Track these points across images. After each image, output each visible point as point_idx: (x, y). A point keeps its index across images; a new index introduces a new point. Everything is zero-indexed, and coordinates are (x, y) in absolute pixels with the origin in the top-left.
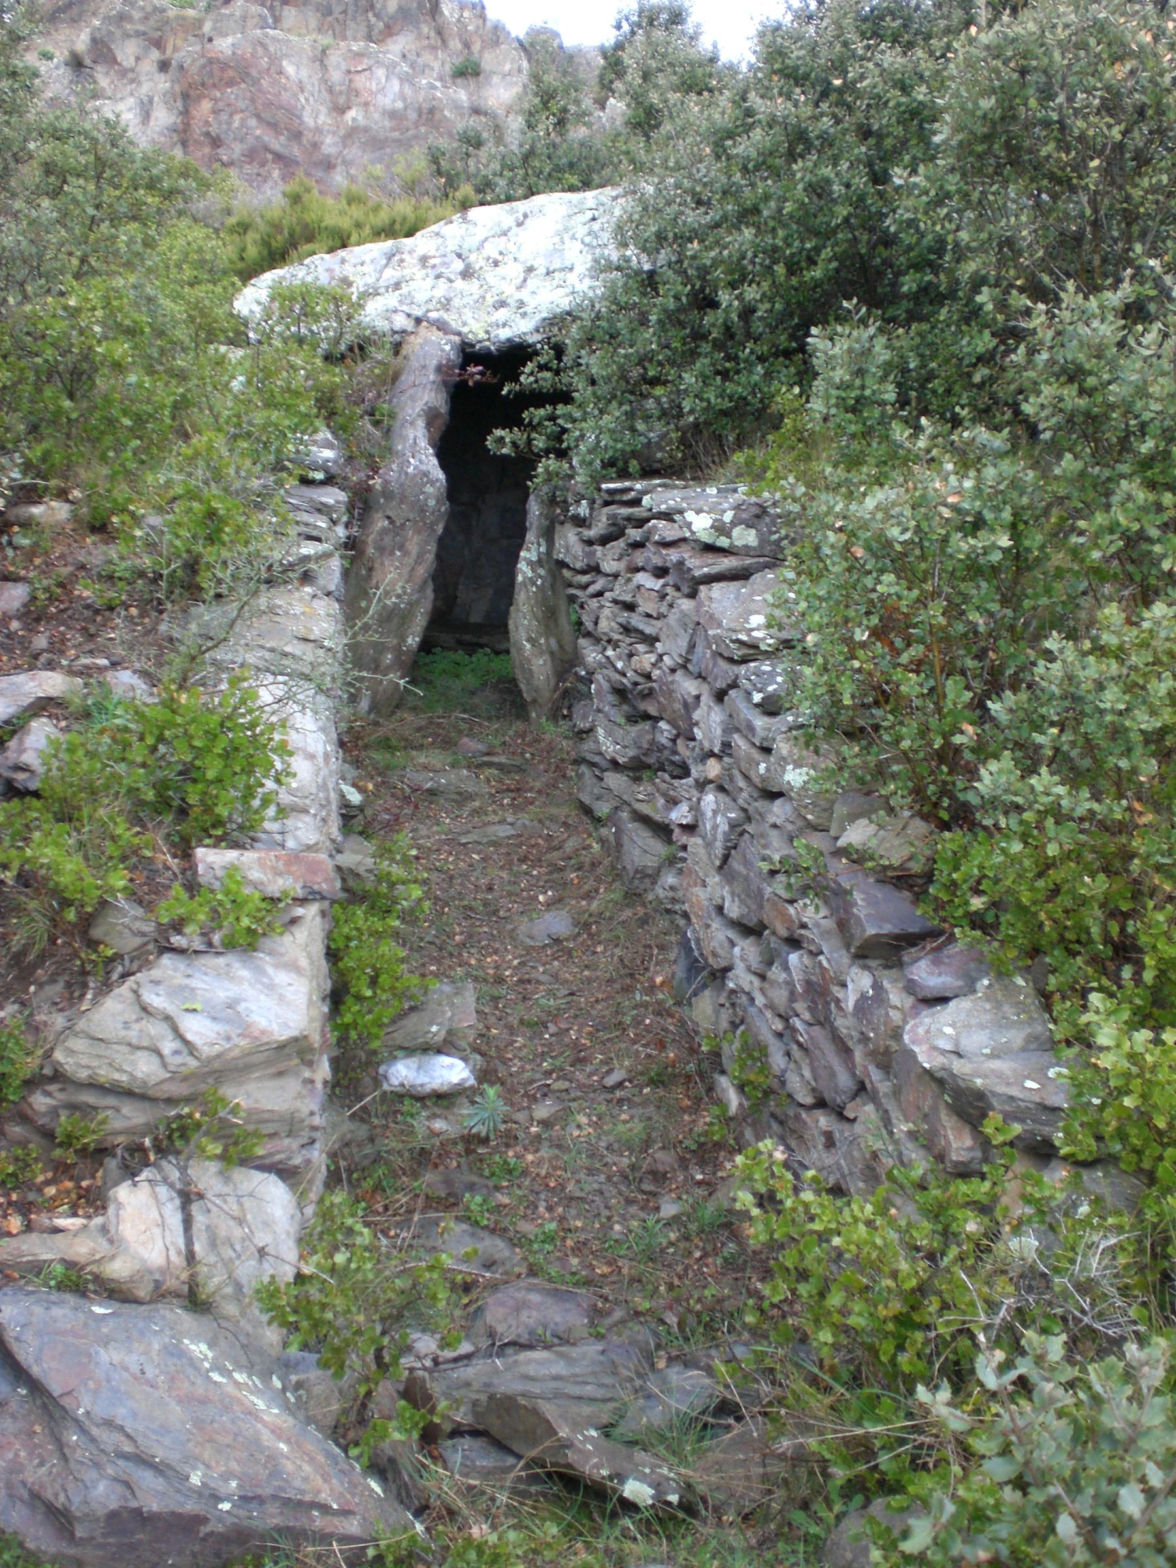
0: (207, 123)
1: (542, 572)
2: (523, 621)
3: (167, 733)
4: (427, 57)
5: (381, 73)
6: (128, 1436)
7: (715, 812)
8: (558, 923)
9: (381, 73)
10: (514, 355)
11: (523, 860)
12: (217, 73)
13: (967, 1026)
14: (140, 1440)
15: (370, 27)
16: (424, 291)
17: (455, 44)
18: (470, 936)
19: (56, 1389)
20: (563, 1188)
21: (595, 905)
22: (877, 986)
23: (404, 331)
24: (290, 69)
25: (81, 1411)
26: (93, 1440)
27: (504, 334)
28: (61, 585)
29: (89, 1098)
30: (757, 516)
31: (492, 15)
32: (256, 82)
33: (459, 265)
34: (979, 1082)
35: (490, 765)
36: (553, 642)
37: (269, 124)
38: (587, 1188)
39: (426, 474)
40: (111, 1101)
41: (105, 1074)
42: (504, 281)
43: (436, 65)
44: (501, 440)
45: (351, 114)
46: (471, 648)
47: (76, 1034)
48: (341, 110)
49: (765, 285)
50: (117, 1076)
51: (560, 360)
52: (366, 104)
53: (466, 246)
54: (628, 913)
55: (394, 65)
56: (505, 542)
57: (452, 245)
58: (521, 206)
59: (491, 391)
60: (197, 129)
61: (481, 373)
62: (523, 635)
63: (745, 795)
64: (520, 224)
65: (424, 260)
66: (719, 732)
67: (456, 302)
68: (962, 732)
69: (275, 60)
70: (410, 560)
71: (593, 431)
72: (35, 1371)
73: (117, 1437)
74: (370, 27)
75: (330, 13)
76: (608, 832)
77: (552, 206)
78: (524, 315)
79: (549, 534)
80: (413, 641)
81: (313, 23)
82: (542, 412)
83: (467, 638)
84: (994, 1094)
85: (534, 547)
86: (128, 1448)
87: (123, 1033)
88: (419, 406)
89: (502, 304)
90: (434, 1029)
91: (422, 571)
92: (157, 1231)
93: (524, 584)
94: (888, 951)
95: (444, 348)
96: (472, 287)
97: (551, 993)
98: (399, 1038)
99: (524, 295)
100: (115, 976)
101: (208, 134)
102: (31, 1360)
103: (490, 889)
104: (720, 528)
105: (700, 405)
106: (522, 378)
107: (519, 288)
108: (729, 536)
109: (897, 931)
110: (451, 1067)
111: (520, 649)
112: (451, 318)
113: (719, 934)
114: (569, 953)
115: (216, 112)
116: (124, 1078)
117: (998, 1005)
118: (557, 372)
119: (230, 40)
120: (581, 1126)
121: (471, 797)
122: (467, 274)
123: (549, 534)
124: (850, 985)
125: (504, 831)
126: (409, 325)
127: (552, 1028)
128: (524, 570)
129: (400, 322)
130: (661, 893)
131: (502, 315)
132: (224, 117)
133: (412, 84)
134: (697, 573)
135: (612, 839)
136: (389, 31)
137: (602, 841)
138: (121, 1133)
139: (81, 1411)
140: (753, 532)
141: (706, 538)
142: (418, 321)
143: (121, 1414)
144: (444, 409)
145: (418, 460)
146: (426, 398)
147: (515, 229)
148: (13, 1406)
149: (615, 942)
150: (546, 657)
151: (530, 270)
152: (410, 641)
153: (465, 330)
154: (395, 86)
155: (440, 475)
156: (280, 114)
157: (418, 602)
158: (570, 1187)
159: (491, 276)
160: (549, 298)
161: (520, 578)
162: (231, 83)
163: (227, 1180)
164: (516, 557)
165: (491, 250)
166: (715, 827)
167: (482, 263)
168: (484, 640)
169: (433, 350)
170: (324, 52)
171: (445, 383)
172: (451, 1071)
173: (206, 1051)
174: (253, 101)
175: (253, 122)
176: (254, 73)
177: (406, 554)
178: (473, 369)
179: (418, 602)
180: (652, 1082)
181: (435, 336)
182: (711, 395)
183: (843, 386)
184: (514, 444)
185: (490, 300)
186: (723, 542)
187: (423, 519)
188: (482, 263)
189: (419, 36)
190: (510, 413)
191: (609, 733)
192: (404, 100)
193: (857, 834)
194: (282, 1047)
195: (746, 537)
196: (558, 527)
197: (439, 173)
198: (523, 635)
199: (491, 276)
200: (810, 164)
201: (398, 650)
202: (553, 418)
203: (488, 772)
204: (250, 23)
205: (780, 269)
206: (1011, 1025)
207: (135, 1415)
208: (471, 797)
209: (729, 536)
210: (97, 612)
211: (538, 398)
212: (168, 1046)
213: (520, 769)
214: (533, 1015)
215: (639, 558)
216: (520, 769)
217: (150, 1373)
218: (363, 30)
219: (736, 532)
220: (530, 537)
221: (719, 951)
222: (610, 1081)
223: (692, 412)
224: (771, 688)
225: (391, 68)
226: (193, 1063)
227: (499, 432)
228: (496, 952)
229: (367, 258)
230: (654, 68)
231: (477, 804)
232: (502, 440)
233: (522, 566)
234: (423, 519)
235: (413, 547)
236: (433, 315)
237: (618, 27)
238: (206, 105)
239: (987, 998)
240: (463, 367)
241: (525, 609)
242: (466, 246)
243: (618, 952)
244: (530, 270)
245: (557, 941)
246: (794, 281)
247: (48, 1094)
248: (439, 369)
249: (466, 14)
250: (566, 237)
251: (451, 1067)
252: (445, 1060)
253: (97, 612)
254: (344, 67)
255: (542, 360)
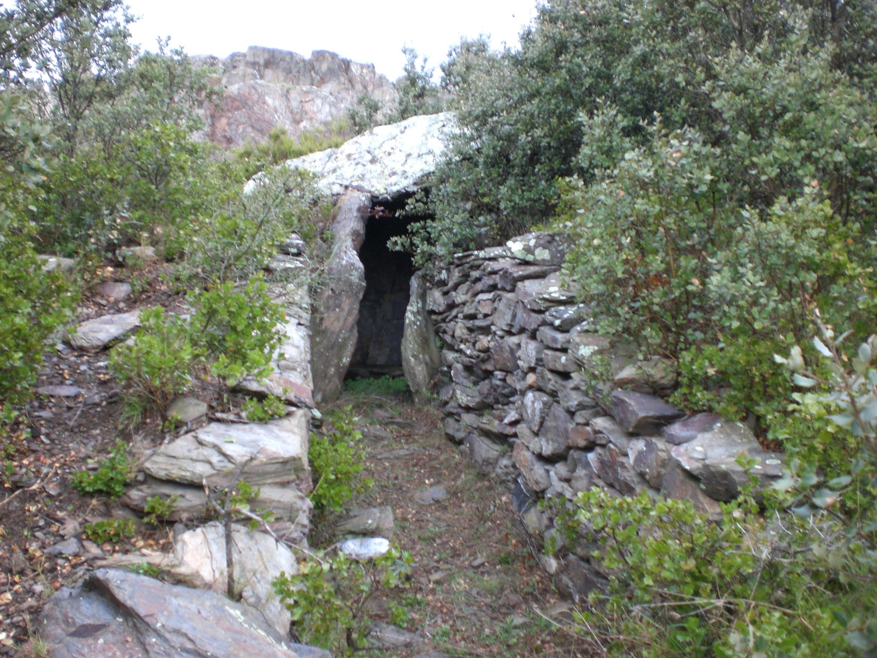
0: (225, 130)
1: (420, 318)
2: (410, 346)
3: (214, 97)
4: (344, 94)
5: (319, 102)
6: (190, 640)
7: (533, 403)
8: (439, 493)
9: (319, 102)
10: (401, 198)
11: (414, 466)
12: (230, 103)
13: (711, 446)
14: (197, 642)
15: (312, 79)
16: (349, 172)
17: (359, 87)
18: (386, 500)
19: (142, 612)
20: (452, 612)
21: (459, 482)
22: (648, 445)
23: (338, 194)
24: (269, 101)
25: (159, 625)
26: (166, 640)
27: (395, 189)
28: (149, 284)
29: (166, 490)
30: (549, 242)
31: (379, 71)
32: (251, 108)
33: (369, 157)
34: (723, 467)
35: (393, 423)
36: (427, 358)
37: (258, 130)
38: (466, 613)
39: (353, 265)
40: (179, 492)
41: (176, 473)
42: (395, 162)
43: (349, 98)
44: (396, 243)
45: (303, 124)
46: (378, 376)
47: (159, 455)
48: (297, 122)
49: (546, 129)
50: (183, 473)
51: (427, 197)
52: (311, 119)
53: (372, 147)
54: (479, 484)
55: (326, 97)
56: (395, 322)
57: (365, 147)
58: (404, 123)
59: (387, 222)
60: (219, 134)
61: (383, 211)
62: (409, 353)
63: (553, 382)
64: (402, 132)
65: (349, 156)
66: (534, 353)
67: (368, 176)
68: (692, 284)
69: (261, 96)
70: (345, 314)
71: (451, 221)
72: (129, 603)
73: (183, 640)
74: (312, 79)
75: (291, 72)
76: (465, 447)
77: (419, 123)
78: (406, 178)
79: (423, 297)
80: (346, 360)
81: (282, 78)
82: (418, 224)
83: (376, 370)
84: (734, 472)
85: (415, 304)
86: (189, 646)
87: (187, 454)
88: (348, 230)
89: (394, 173)
90: (370, 521)
91: (351, 320)
92: (208, 561)
93: (410, 324)
94: (654, 427)
95: (362, 199)
96: (377, 167)
97: (435, 526)
98: (350, 525)
99: (406, 168)
100: (182, 432)
101: (225, 137)
102: (127, 597)
103: (396, 478)
104: (528, 250)
105: (510, 204)
106: (407, 208)
107: (403, 165)
108: (533, 254)
109: (658, 414)
110: (381, 544)
111: (408, 361)
112: (365, 185)
113: (539, 469)
114: (445, 508)
115: (229, 124)
116: (188, 474)
117: (728, 435)
118: (426, 203)
119: (237, 86)
120: (461, 584)
121: (382, 439)
122: (373, 161)
123: (423, 297)
124: (630, 452)
125: (402, 452)
126: (341, 190)
127: (438, 541)
128: (409, 316)
129: (337, 189)
130: (499, 470)
131: (394, 179)
132: (234, 127)
133: (335, 107)
134: (515, 275)
135: (467, 450)
136: (323, 81)
137: (462, 453)
138: (184, 511)
139: (159, 625)
140: (547, 251)
141: (519, 255)
142: (346, 187)
143: (185, 628)
144: (362, 232)
145: (348, 257)
146: (352, 225)
147: (400, 135)
148: (113, 627)
149: (470, 499)
150: (423, 365)
151: (409, 155)
152: (344, 360)
153: (373, 189)
154: (327, 108)
155: (361, 265)
156: (264, 125)
157: (349, 338)
158: (456, 612)
159: (387, 160)
160: (418, 168)
161: (407, 321)
162: (237, 109)
163: (252, 537)
164: (405, 311)
165: (387, 147)
166: (534, 410)
167: (382, 155)
168: (385, 371)
169: (356, 200)
170: (288, 92)
171: (362, 218)
172: (379, 546)
173: (239, 459)
174: (249, 118)
175: (249, 129)
176: (250, 103)
177: (342, 310)
178: (378, 208)
179: (349, 338)
180: (500, 563)
181: (356, 194)
182: (517, 199)
183: (602, 139)
184: (402, 244)
185: (387, 172)
186: (530, 258)
187: (351, 290)
188: (382, 155)
189: (339, 83)
190: (400, 227)
191: (463, 392)
192: (332, 115)
193: (628, 372)
194: (285, 462)
195: (543, 254)
196: (428, 292)
197: (355, 124)
198: (409, 353)
199: (387, 160)
200: (569, 57)
201: (338, 367)
202: (424, 228)
203: (391, 427)
204: (247, 78)
205: (554, 121)
206: (736, 444)
207: (194, 629)
208: (382, 439)
209: (533, 254)
210: (170, 296)
211: (416, 218)
212: (215, 458)
213: (410, 425)
214: (427, 534)
215: (479, 286)
216: (410, 425)
217: (204, 613)
218: (309, 81)
219: (537, 252)
220: (413, 299)
221: (540, 480)
222: (476, 563)
223: (505, 209)
224: (565, 316)
225: (324, 99)
226: (231, 466)
227: (394, 239)
228: (402, 507)
229: (317, 159)
230: (470, 60)
231: (386, 442)
232: (396, 243)
233: (408, 315)
234: (351, 290)
235: (346, 308)
236: (355, 184)
237: (450, 55)
238: (224, 121)
239: (721, 432)
240: (373, 208)
241: (410, 338)
242: (372, 147)
243: (474, 505)
244: (409, 155)
245: (437, 502)
246: (562, 128)
247: (141, 490)
248: (359, 210)
249: (365, 71)
250: (429, 137)
251: (381, 544)
252: (378, 540)
253: (170, 296)
254: (299, 99)
255: (418, 197)
